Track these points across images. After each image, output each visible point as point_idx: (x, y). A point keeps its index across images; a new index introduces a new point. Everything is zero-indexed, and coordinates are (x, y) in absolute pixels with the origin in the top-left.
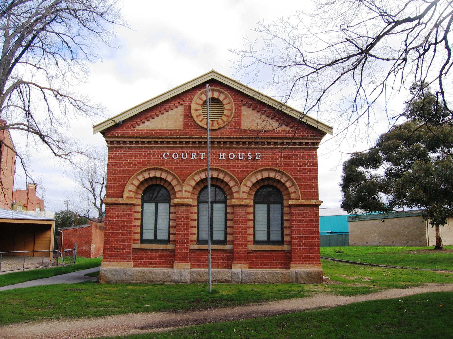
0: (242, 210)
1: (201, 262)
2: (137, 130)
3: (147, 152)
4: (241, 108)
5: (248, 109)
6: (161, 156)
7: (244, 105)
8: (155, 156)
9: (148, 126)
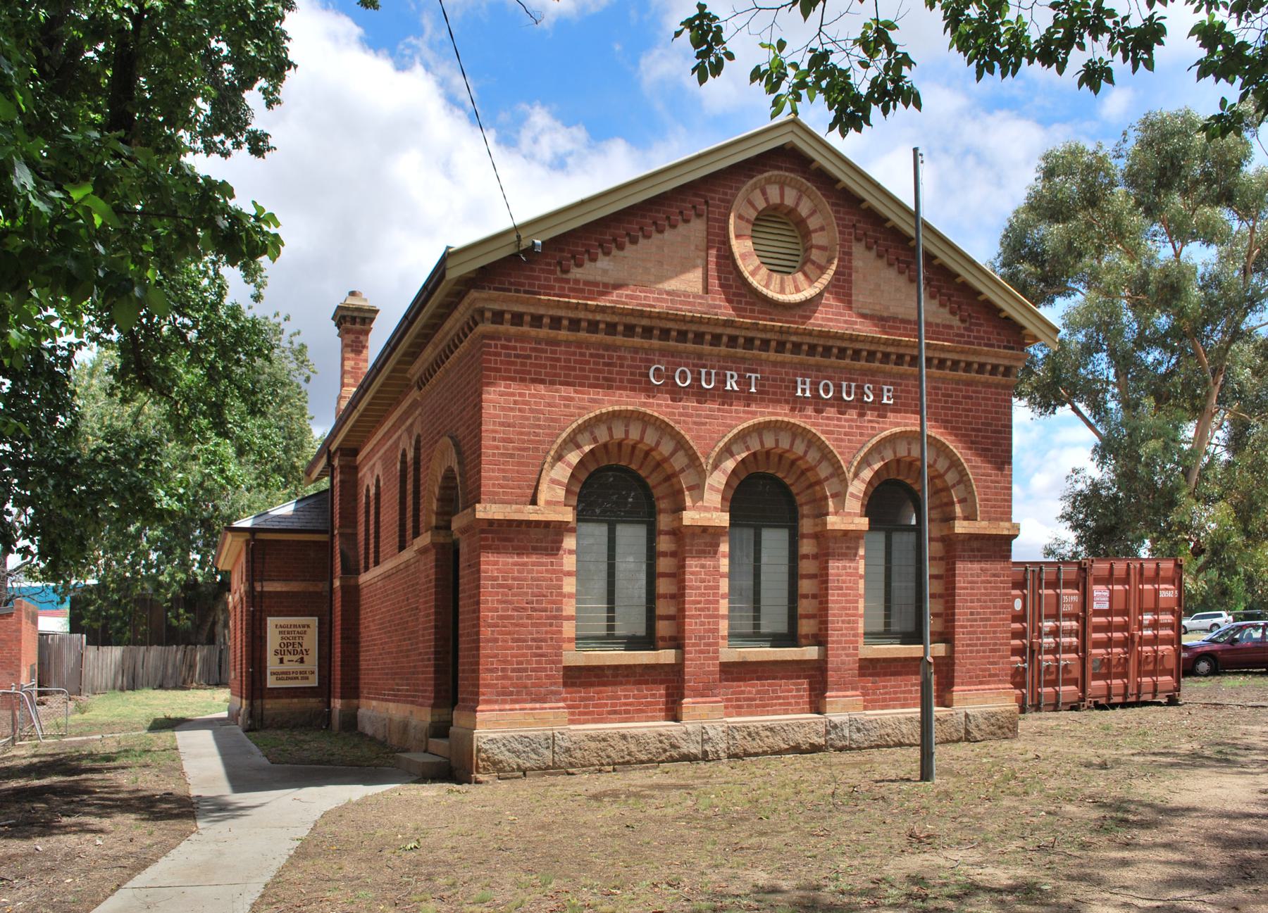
0: (848, 548)
1: (745, 699)
2: (577, 281)
3: (603, 357)
4: (850, 247)
5: (867, 253)
6: (641, 375)
7: (858, 240)
8: (625, 374)
9: (605, 272)
